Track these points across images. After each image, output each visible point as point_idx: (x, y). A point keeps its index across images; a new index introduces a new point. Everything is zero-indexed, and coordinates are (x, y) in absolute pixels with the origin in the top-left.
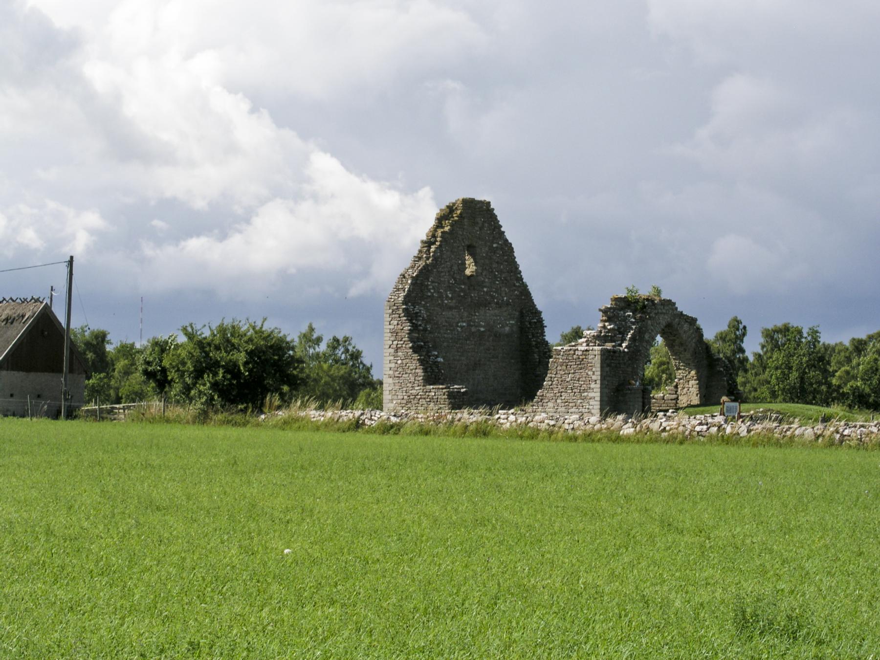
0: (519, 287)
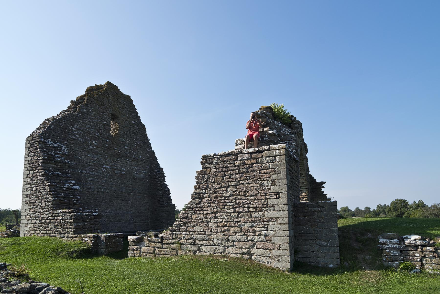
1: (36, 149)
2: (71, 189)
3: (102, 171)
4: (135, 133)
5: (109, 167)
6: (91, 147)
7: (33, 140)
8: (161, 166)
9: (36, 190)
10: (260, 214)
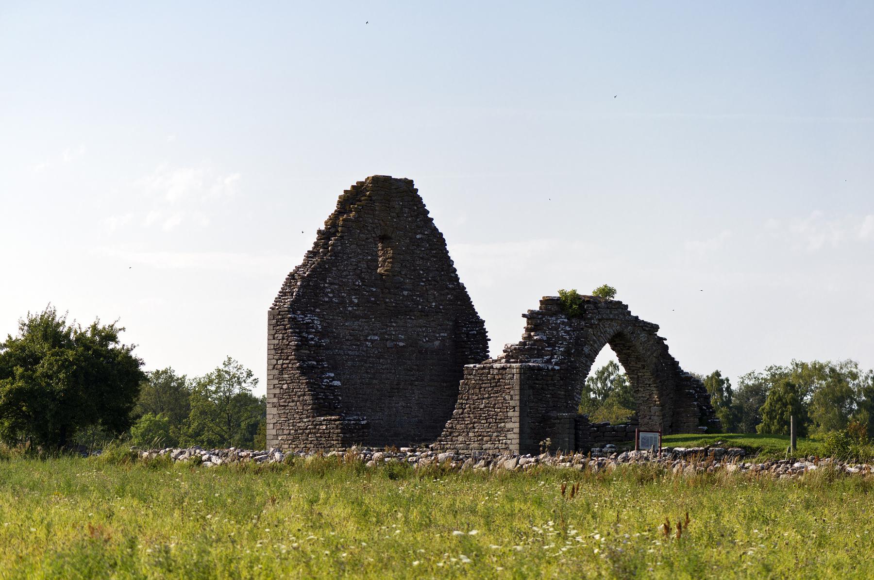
0: (453, 289)
1: (286, 329)
2: (331, 386)
3: (367, 346)
4: (422, 258)
5: (376, 338)
6: (350, 309)
7: (279, 314)
8: (482, 315)
9: (288, 388)
10: (503, 424)
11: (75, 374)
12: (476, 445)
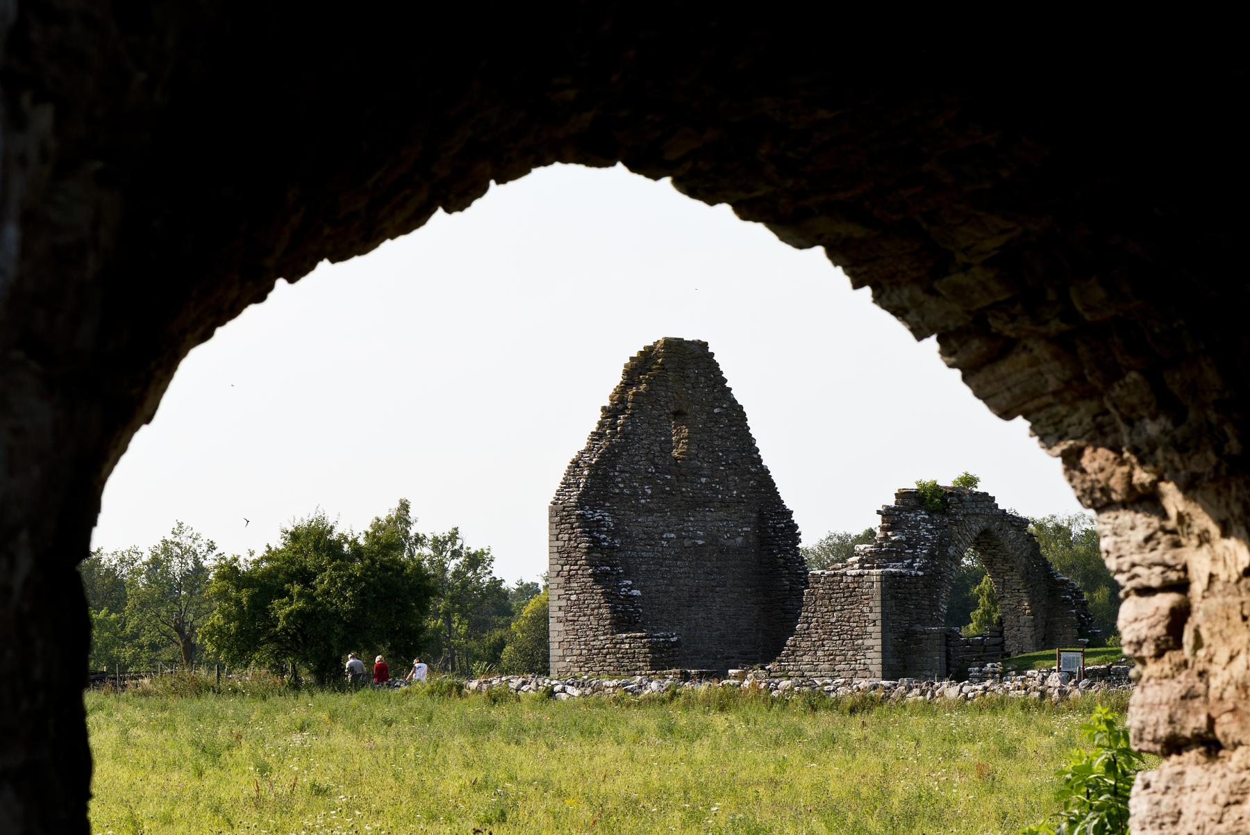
0: (756, 473)
4: (721, 437)
8: (788, 505)
9: (578, 600)
10: (860, 642)
11: (362, 593)
12: (826, 666)
